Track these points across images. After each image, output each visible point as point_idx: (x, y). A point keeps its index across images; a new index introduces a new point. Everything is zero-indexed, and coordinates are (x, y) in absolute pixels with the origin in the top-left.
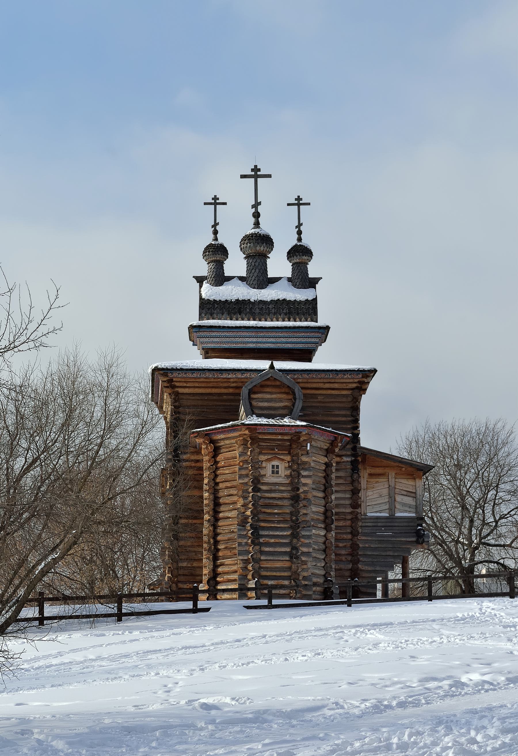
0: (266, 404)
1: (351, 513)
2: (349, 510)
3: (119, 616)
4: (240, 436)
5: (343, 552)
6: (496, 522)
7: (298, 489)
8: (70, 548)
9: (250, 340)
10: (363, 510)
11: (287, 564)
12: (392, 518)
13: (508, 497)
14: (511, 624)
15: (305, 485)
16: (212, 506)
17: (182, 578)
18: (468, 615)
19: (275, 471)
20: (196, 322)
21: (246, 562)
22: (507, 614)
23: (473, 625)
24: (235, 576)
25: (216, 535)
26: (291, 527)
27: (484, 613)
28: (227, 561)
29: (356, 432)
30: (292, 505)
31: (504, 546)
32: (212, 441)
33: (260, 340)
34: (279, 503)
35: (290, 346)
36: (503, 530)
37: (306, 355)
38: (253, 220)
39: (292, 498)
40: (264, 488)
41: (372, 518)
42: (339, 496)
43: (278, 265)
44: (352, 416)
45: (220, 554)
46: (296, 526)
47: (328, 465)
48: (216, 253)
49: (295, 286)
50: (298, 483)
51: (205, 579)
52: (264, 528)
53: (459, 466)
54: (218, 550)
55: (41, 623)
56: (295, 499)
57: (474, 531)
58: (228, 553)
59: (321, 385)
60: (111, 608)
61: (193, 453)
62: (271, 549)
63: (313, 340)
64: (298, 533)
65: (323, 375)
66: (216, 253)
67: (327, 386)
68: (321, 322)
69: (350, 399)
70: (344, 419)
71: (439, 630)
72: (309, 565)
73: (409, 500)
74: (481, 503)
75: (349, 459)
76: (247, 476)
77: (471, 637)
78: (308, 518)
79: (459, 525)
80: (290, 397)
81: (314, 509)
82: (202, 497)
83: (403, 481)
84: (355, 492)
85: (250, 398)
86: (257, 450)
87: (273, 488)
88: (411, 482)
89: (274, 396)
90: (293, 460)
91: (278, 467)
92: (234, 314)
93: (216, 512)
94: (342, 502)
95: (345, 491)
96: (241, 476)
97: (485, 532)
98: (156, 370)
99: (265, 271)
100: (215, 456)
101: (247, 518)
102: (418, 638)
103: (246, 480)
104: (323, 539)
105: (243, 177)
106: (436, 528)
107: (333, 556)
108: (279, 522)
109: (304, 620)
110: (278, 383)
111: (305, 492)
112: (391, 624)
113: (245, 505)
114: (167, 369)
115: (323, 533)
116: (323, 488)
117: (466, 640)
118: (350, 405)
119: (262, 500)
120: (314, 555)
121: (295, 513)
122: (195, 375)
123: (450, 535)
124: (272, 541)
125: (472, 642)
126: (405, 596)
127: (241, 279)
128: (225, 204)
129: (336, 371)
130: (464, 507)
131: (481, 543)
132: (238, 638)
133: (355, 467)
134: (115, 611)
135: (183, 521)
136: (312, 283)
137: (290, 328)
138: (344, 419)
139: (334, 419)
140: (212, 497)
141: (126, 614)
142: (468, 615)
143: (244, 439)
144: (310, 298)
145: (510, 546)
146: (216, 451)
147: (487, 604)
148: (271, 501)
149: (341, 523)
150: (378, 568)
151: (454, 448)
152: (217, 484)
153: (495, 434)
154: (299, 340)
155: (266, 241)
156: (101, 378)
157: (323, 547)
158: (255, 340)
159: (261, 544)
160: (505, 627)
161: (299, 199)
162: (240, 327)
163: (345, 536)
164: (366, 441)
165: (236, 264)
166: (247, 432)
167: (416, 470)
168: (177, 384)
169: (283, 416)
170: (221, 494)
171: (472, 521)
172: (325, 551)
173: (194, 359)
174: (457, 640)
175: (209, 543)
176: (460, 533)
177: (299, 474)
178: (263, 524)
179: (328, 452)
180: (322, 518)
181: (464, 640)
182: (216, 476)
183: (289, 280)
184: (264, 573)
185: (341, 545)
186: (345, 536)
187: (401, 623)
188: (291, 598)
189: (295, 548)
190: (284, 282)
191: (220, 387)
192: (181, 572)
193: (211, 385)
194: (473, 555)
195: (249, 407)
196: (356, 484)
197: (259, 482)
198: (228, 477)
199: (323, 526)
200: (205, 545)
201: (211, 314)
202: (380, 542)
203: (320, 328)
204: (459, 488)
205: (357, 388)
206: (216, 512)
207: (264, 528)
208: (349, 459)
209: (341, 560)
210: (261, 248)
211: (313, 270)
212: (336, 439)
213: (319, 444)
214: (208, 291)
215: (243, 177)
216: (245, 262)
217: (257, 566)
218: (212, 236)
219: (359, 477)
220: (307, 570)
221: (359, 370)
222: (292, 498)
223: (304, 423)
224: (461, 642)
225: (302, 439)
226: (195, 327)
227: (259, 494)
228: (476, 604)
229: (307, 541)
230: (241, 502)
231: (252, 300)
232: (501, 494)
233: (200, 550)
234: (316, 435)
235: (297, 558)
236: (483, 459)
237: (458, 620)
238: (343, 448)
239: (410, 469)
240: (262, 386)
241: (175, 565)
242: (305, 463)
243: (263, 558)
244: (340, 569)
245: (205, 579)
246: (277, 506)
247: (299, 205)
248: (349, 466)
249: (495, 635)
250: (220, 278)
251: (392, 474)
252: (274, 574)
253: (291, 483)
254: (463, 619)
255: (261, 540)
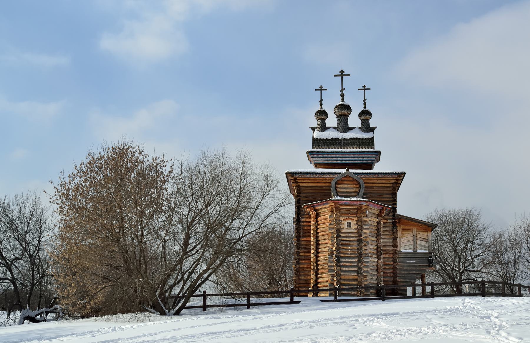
0: (344, 190)
1: (393, 250)
2: (391, 248)
3: (249, 305)
4: (330, 206)
5: (389, 271)
6: (472, 259)
7: (361, 236)
8: (212, 264)
9: (339, 159)
10: (399, 248)
11: (356, 277)
12: (415, 253)
13: (478, 247)
14: (486, 316)
15: (365, 233)
16: (315, 245)
17: (301, 285)
18: (454, 307)
19: (349, 226)
20: (310, 149)
21: (333, 276)
22: (482, 307)
23: (457, 315)
24: (327, 284)
25: (317, 261)
26: (358, 257)
27: (466, 307)
28: (323, 276)
29: (395, 206)
30: (358, 245)
31: (477, 271)
32: (315, 210)
33: (344, 159)
34: (351, 243)
35: (360, 162)
36: (476, 263)
37: (369, 166)
38: (341, 98)
39: (358, 241)
40: (343, 235)
41: (404, 253)
42: (385, 241)
43: (354, 120)
44: (393, 198)
45: (320, 271)
46: (360, 256)
47: (379, 223)
48: (322, 114)
49: (362, 131)
50: (362, 232)
51: (312, 285)
52: (343, 257)
53: (453, 232)
54: (318, 269)
55: (204, 310)
56: (360, 241)
57: (461, 264)
58: (323, 271)
59: (376, 181)
60: (245, 301)
61: (307, 218)
62: (347, 269)
63: (372, 159)
64: (361, 260)
65: (376, 176)
66: (322, 114)
67: (379, 181)
68: (376, 149)
69: (391, 189)
70: (388, 199)
71: (430, 320)
72: (368, 278)
73: (424, 243)
74: (464, 250)
75: (391, 221)
76: (333, 228)
77: (454, 328)
78: (367, 252)
79: (454, 261)
80: (358, 186)
81: (371, 247)
82: (310, 241)
83: (421, 233)
84: (395, 239)
85: (336, 187)
86: (339, 214)
87: (348, 235)
88: (425, 234)
89: (349, 186)
90: (358, 220)
91: (350, 223)
92: (331, 145)
93: (317, 249)
94: (388, 244)
95: (389, 238)
96: (330, 229)
97: (467, 264)
98: (287, 174)
99: (347, 124)
100: (317, 218)
101: (333, 251)
102: (408, 328)
103: (333, 231)
104: (376, 264)
105: (335, 76)
106: (442, 262)
107: (382, 273)
108: (351, 254)
109: (347, 309)
110: (351, 179)
111: (365, 237)
112: (397, 314)
113: (332, 245)
114: (293, 173)
115: (376, 260)
116: (376, 235)
117: (449, 331)
118: (391, 192)
119: (341, 242)
120: (371, 272)
121: (360, 249)
122: (308, 176)
123: (449, 266)
124: (347, 264)
125: (453, 333)
126: (424, 295)
127: (335, 128)
128: (326, 90)
129: (383, 173)
130: (455, 251)
131: (464, 270)
132: (282, 323)
133: (394, 224)
134: (201, 304)
135: (302, 254)
136: (372, 130)
137: (359, 152)
138: (388, 199)
139: (383, 199)
140: (315, 240)
141: (209, 306)
142: (454, 307)
143: (332, 208)
144: (370, 137)
145: (480, 271)
146: (317, 215)
147: (467, 299)
148: (347, 242)
149: (387, 256)
150: (408, 280)
151: (449, 222)
152: (318, 233)
153: (471, 215)
154: (365, 159)
155: (347, 108)
156: (239, 165)
157: (376, 268)
158: (341, 159)
159: (341, 266)
160: (482, 318)
161: (364, 86)
162: (333, 152)
163: (389, 263)
164: (401, 210)
165: (332, 121)
166: (333, 204)
167: (428, 226)
168: (299, 181)
169: (353, 197)
170: (320, 238)
171: (460, 259)
172: (377, 270)
173: (311, 168)
174: (441, 331)
175: (313, 265)
176: (454, 265)
177: (362, 227)
178: (342, 255)
179: (379, 216)
180: (375, 252)
181: (447, 331)
182: (317, 229)
183: (360, 128)
184: (343, 282)
185: (387, 267)
186: (389, 263)
187: (404, 314)
188: (358, 296)
189: (360, 268)
190: (357, 130)
191: (322, 183)
192: (301, 282)
193: (317, 181)
194: (461, 276)
195: (335, 191)
196: (395, 234)
197: (340, 232)
198: (324, 229)
199: (376, 256)
200: (312, 267)
201: (319, 146)
202: (409, 266)
203: (375, 152)
204: (453, 242)
205: (395, 182)
206: (317, 249)
207: (343, 257)
208: (391, 221)
209: (388, 276)
210: (345, 112)
211: (372, 123)
212: (383, 208)
213: (373, 211)
214: (317, 134)
215: (335, 76)
216: (337, 119)
217: (339, 278)
218: (320, 107)
219: (397, 230)
220: (367, 281)
221: (396, 173)
222: (358, 241)
223: (364, 200)
224: (444, 333)
225: (363, 208)
226: (310, 152)
227: (340, 238)
228: (460, 300)
229: (366, 265)
230: (330, 243)
231: (340, 138)
232: (474, 245)
233: (309, 269)
234: (371, 206)
235: (361, 274)
236: (465, 227)
237: (447, 312)
238: (388, 214)
239: (424, 226)
240: (342, 181)
241: (297, 278)
242: (365, 221)
243: (342, 274)
244: (387, 281)
245: (312, 285)
246: (350, 245)
247: (364, 89)
248: (391, 225)
249: (475, 326)
250: (323, 128)
251: (415, 229)
252: (349, 283)
253: (358, 233)
254: (450, 311)
255: (341, 264)
